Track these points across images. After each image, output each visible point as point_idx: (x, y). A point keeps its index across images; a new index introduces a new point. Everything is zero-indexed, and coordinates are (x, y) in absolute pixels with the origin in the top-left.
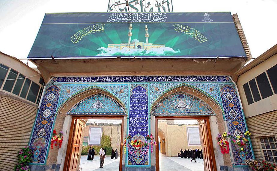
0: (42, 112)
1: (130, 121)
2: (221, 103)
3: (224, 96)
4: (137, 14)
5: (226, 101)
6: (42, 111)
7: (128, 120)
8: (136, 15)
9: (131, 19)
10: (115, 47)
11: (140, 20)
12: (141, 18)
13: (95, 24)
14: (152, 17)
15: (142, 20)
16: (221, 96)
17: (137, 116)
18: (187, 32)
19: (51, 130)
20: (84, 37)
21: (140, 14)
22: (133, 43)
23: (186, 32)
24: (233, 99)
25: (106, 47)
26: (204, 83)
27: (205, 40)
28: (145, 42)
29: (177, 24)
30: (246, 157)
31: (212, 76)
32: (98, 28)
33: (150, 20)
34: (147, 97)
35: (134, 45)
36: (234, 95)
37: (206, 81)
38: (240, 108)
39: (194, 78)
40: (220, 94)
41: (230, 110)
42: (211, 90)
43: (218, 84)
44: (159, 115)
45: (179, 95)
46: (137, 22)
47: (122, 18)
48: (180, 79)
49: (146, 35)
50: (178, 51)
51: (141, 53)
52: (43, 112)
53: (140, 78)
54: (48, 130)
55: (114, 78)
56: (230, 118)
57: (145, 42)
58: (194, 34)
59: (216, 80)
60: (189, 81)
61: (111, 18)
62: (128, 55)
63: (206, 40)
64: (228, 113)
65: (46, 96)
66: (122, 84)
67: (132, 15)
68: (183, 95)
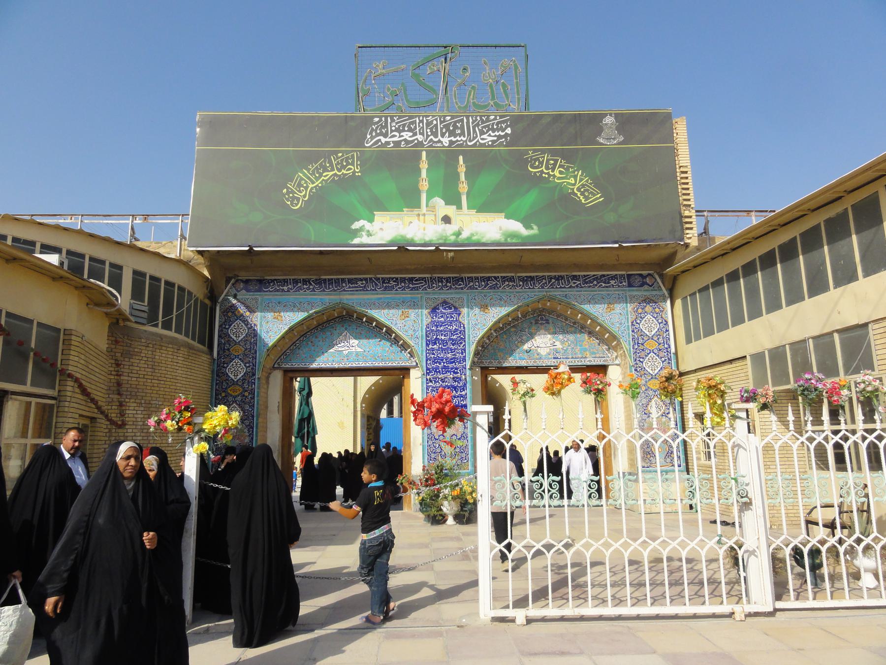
0: (224, 367)
1: (428, 383)
2: (629, 341)
3: (637, 323)
4: (436, 120)
5: (642, 335)
6: (224, 364)
7: (422, 382)
8: (435, 122)
9: (421, 136)
10: (390, 220)
11: (446, 141)
12: (447, 134)
13: (336, 152)
14: (474, 131)
15: (450, 139)
16: (630, 324)
17: (442, 371)
18: (557, 174)
19: (254, 406)
20: (314, 190)
21: (444, 119)
22: (432, 209)
23: (554, 176)
24: (656, 330)
25: (371, 220)
26: (596, 291)
27: (598, 198)
28: (459, 207)
29: (535, 151)
30: (666, 453)
31: (616, 275)
32: (345, 164)
33: (470, 141)
34: (464, 328)
35: (435, 215)
36: (660, 321)
37: (599, 286)
38: (669, 350)
39: (572, 280)
40: (628, 318)
41: (646, 356)
42: (609, 310)
43: (628, 294)
44: (490, 365)
45: (537, 318)
46: (439, 145)
47: (402, 134)
48: (539, 283)
49: (461, 185)
50: (533, 229)
51: (451, 235)
52: (226, 368)
53: (447, 281)
54: (247, 407)
55: (383, 282)
56: (645, 374)
57: (459, 207)
58: (573, 182)
59: (624, 284)
60: (561, 287)
61: (374, 134)
62: (423, 242)
63: (600, 197)
64: (641, 362)
65: (225, 328)
66: (403, 298)
67: (425, 121)
68: (547, 317)
